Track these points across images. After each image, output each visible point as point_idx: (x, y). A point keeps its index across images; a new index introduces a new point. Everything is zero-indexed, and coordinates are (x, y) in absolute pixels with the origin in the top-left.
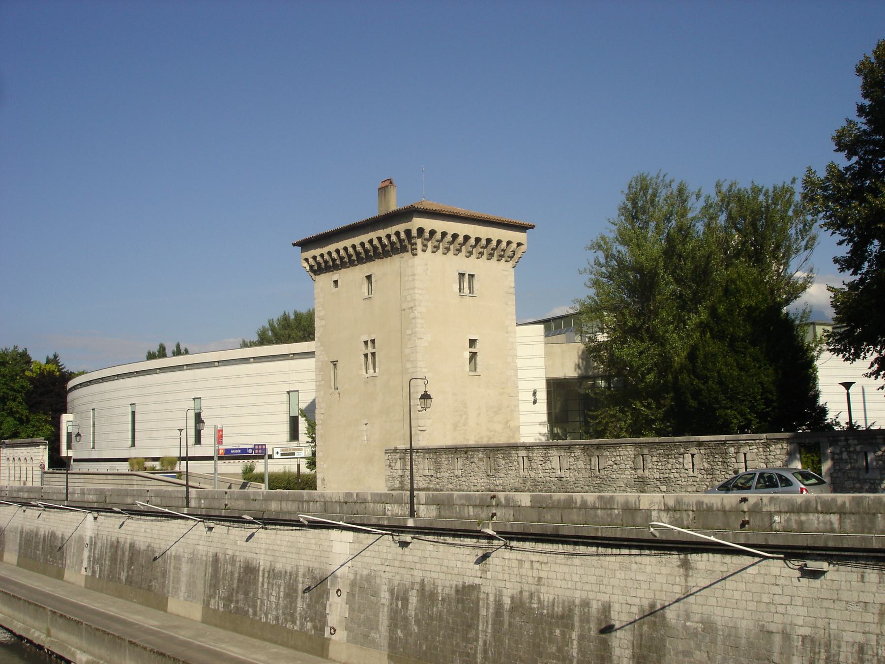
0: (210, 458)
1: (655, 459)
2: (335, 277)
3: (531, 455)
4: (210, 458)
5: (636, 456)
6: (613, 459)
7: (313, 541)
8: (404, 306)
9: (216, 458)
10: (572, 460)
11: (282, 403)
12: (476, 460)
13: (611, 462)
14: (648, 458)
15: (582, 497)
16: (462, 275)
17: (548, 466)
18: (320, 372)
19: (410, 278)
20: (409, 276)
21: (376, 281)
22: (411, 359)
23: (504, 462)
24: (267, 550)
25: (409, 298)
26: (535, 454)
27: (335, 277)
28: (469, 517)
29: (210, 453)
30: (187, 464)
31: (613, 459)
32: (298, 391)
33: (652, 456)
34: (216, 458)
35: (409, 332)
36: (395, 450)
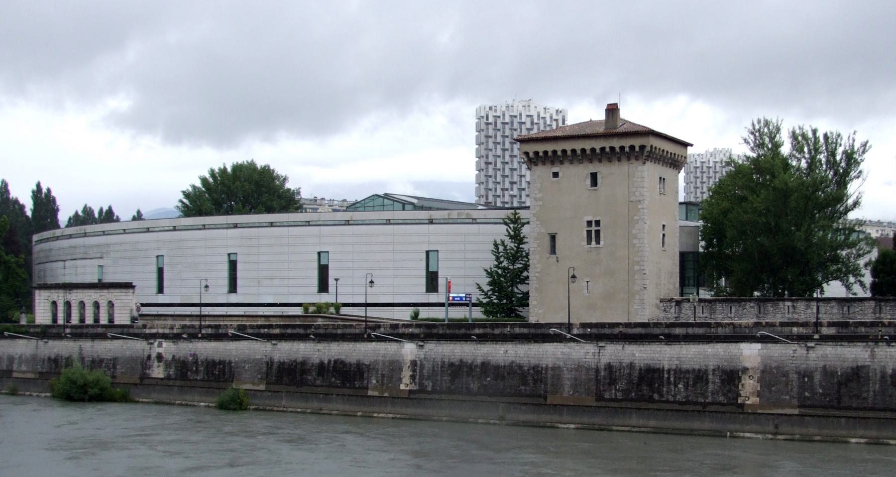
0: (442, 305)
1: (888, 308)
2: (555, 170)
3: (795, 305)
4: (442, 305)
5: (876, 306)
6: (860, 308)
7: (722, 350)
8: (632, 199)
9: (446, 305)
10: (828, 308)
11: (421, 260)
12: (747, 307)
13: (858, 310)
14: (884, 308)
15: (81, 349)
16: (660, 178)
17: (809, 311)
18: (535, 240)
19: (639, 180)
20: (638, 178)
21: (602, 177)
22: (639, 237)
23: (772, 309)
24: (677, 357)
25: (637, 194)
26: (798, 305)
27: (555, 170)
28: (862, 332)
29: (442, 300)
30: (201, 309)
31: (860, 308)
32: (438, 251)
33: (887, 306)
34: (446, 305)
35: (636, 218)
36: (671, 300)
